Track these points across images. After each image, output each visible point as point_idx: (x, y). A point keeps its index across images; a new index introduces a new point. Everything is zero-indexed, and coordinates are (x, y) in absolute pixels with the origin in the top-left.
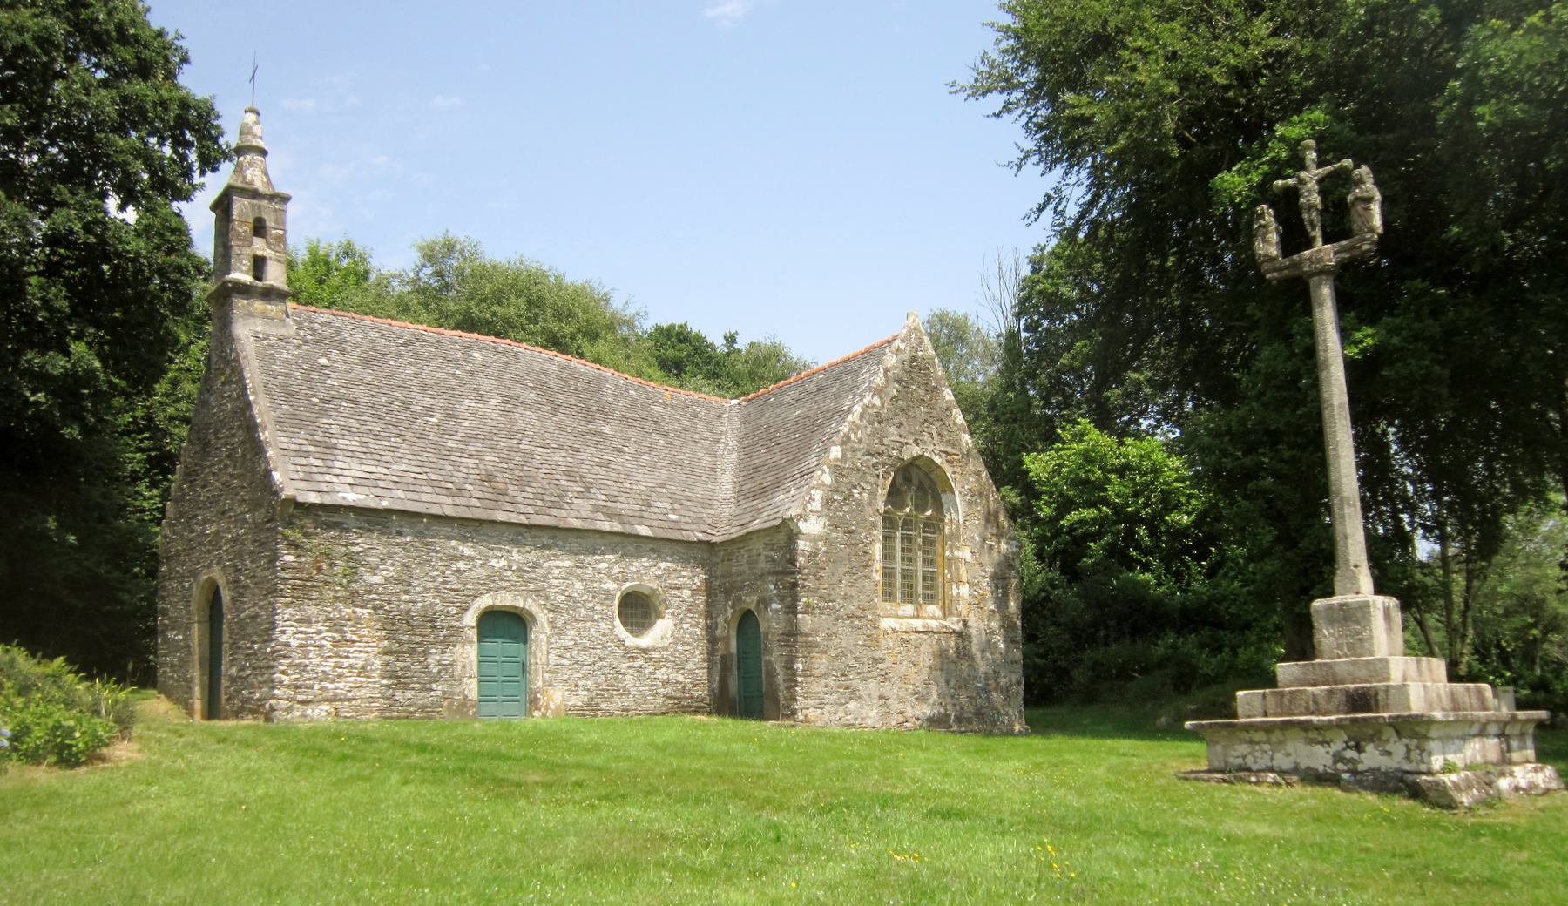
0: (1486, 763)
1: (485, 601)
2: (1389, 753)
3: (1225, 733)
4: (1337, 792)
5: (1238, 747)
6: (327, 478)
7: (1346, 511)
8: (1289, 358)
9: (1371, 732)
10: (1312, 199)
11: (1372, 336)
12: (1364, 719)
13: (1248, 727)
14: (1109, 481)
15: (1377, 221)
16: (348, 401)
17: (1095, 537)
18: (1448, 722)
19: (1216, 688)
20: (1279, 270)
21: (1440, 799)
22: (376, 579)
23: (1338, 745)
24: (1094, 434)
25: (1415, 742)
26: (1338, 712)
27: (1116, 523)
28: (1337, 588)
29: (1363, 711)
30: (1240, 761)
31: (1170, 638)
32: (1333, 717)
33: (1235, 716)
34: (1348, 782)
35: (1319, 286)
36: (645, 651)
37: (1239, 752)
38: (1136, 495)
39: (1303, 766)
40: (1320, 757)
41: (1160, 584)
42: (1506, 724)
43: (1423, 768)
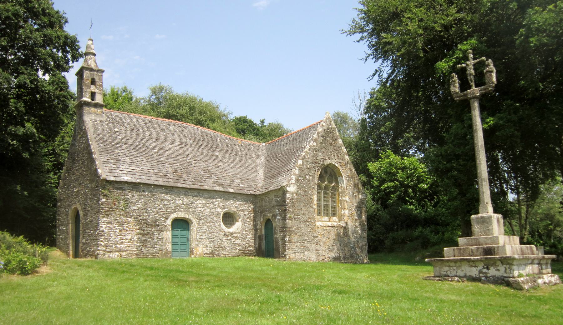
0: (534, 274)
1: (174, 216)
2: (499, 270)
3: (440, 263)
4: (480, 284)
5: (444, 268)
6: (118, 171)
7: (483, 183)
8: (463, 129)
9: (492, 262)
10: (471, 71)
11: (493, 121)
12: (490, 258)
13: (448, 261)
14: (398, 173)
15: (494, 79)
16: (125, 144)
17: (393, 193)
18: (520, 259)
19: (437, 247)
20: (459, 97)
21: (517, 287)
22: (135, 208)
23: (480, 267)
24: (393, 156)
25: (508, 266)
26: (480, 255)
27: (401, 188)
28: (480, 211)
29: (489, 255)
30: (445, 273)
31: (420, 229)
32: (479, 257)
33: (443, 257)
34: (484, 280)
35: (474, 103)
36: (232, 233)
37: (445, 270)
38: (408, 177)
39: (468, 275)
40: (474, 272)
41: (416, 210)
42: (541, 260)
43: (511, 275)
